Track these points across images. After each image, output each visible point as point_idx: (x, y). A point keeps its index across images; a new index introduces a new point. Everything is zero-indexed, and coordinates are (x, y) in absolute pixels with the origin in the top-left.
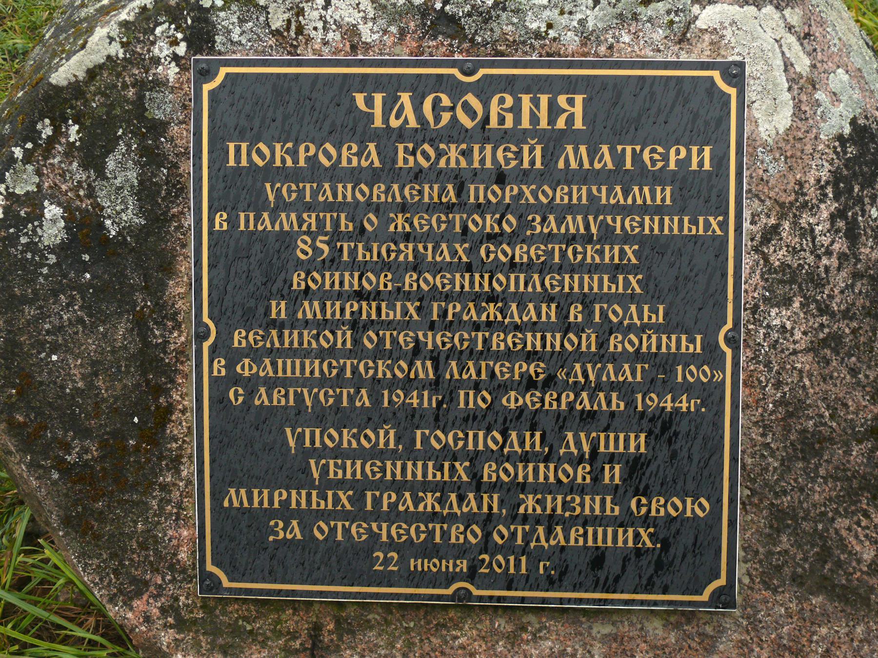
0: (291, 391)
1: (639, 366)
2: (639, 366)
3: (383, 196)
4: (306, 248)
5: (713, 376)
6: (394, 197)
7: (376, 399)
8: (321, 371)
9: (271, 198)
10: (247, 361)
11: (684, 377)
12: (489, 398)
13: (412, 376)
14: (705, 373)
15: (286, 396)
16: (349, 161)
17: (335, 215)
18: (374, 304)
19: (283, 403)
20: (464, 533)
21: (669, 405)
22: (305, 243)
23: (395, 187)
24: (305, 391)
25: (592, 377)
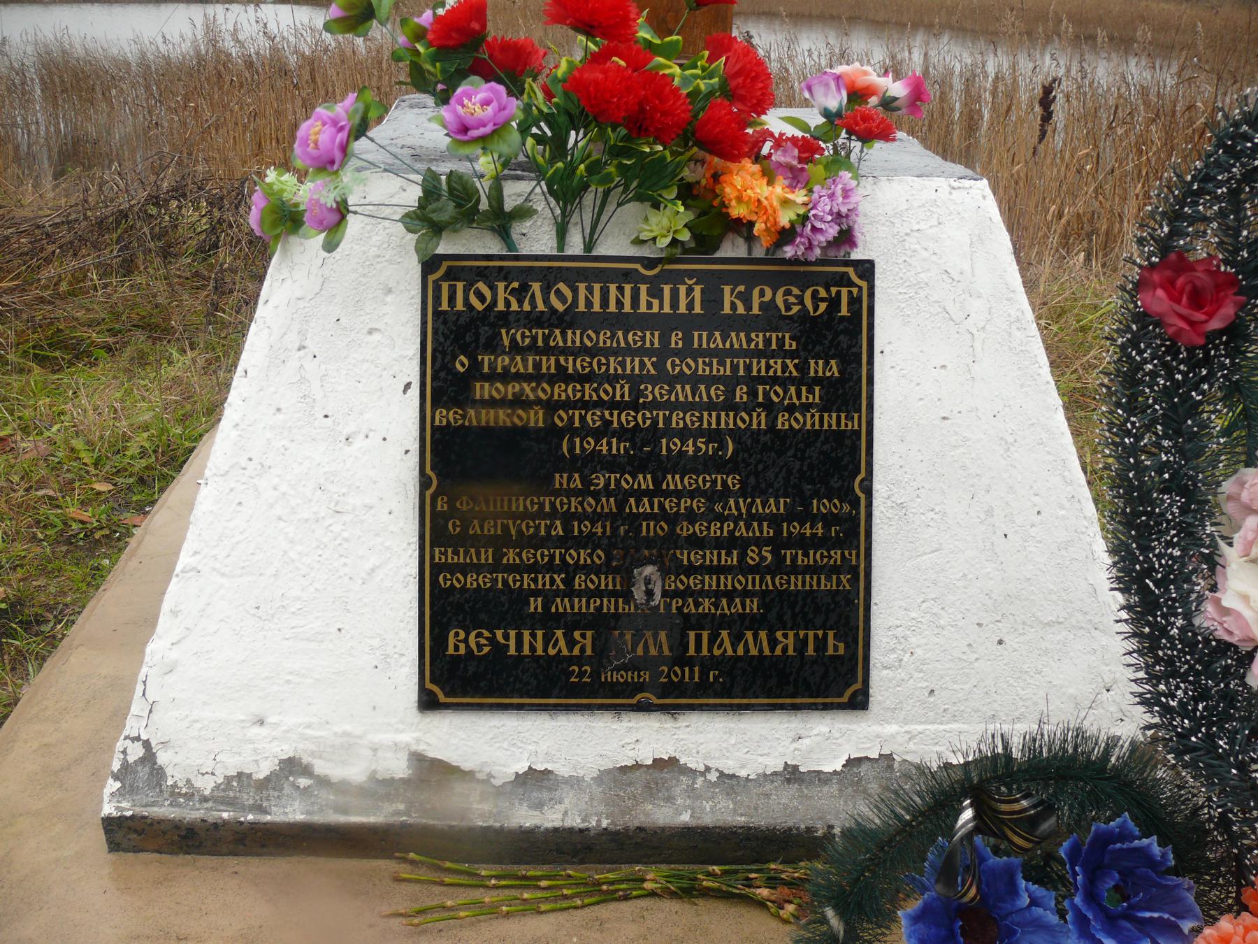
0: (499, 522)
1: (782, 501)
2: (782, 501)
3: (609, 342)
4: (754, 556)
5: (842, 507)
6: (618, 342)
7: (567, 528)
8: (525, 507)
9: (506, 343)
10: (465, 498)
11: (818, 509)
12: (666, 527)
13: (599, 510)
14: (835, 506)
15: (495, 526)
16: (605, 342)
17: (820, 633)
18: (800, 577)
19: (718, 534)
20: (675, 582)
21: (808, 532)
22: (753, 551)
23: (620, 333)
24: (511, 522)
25: (744, 511)
